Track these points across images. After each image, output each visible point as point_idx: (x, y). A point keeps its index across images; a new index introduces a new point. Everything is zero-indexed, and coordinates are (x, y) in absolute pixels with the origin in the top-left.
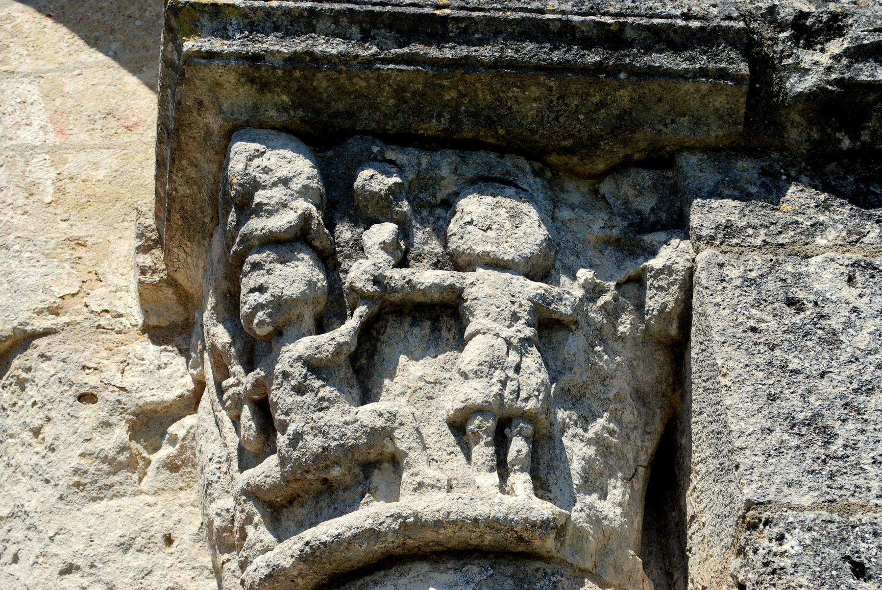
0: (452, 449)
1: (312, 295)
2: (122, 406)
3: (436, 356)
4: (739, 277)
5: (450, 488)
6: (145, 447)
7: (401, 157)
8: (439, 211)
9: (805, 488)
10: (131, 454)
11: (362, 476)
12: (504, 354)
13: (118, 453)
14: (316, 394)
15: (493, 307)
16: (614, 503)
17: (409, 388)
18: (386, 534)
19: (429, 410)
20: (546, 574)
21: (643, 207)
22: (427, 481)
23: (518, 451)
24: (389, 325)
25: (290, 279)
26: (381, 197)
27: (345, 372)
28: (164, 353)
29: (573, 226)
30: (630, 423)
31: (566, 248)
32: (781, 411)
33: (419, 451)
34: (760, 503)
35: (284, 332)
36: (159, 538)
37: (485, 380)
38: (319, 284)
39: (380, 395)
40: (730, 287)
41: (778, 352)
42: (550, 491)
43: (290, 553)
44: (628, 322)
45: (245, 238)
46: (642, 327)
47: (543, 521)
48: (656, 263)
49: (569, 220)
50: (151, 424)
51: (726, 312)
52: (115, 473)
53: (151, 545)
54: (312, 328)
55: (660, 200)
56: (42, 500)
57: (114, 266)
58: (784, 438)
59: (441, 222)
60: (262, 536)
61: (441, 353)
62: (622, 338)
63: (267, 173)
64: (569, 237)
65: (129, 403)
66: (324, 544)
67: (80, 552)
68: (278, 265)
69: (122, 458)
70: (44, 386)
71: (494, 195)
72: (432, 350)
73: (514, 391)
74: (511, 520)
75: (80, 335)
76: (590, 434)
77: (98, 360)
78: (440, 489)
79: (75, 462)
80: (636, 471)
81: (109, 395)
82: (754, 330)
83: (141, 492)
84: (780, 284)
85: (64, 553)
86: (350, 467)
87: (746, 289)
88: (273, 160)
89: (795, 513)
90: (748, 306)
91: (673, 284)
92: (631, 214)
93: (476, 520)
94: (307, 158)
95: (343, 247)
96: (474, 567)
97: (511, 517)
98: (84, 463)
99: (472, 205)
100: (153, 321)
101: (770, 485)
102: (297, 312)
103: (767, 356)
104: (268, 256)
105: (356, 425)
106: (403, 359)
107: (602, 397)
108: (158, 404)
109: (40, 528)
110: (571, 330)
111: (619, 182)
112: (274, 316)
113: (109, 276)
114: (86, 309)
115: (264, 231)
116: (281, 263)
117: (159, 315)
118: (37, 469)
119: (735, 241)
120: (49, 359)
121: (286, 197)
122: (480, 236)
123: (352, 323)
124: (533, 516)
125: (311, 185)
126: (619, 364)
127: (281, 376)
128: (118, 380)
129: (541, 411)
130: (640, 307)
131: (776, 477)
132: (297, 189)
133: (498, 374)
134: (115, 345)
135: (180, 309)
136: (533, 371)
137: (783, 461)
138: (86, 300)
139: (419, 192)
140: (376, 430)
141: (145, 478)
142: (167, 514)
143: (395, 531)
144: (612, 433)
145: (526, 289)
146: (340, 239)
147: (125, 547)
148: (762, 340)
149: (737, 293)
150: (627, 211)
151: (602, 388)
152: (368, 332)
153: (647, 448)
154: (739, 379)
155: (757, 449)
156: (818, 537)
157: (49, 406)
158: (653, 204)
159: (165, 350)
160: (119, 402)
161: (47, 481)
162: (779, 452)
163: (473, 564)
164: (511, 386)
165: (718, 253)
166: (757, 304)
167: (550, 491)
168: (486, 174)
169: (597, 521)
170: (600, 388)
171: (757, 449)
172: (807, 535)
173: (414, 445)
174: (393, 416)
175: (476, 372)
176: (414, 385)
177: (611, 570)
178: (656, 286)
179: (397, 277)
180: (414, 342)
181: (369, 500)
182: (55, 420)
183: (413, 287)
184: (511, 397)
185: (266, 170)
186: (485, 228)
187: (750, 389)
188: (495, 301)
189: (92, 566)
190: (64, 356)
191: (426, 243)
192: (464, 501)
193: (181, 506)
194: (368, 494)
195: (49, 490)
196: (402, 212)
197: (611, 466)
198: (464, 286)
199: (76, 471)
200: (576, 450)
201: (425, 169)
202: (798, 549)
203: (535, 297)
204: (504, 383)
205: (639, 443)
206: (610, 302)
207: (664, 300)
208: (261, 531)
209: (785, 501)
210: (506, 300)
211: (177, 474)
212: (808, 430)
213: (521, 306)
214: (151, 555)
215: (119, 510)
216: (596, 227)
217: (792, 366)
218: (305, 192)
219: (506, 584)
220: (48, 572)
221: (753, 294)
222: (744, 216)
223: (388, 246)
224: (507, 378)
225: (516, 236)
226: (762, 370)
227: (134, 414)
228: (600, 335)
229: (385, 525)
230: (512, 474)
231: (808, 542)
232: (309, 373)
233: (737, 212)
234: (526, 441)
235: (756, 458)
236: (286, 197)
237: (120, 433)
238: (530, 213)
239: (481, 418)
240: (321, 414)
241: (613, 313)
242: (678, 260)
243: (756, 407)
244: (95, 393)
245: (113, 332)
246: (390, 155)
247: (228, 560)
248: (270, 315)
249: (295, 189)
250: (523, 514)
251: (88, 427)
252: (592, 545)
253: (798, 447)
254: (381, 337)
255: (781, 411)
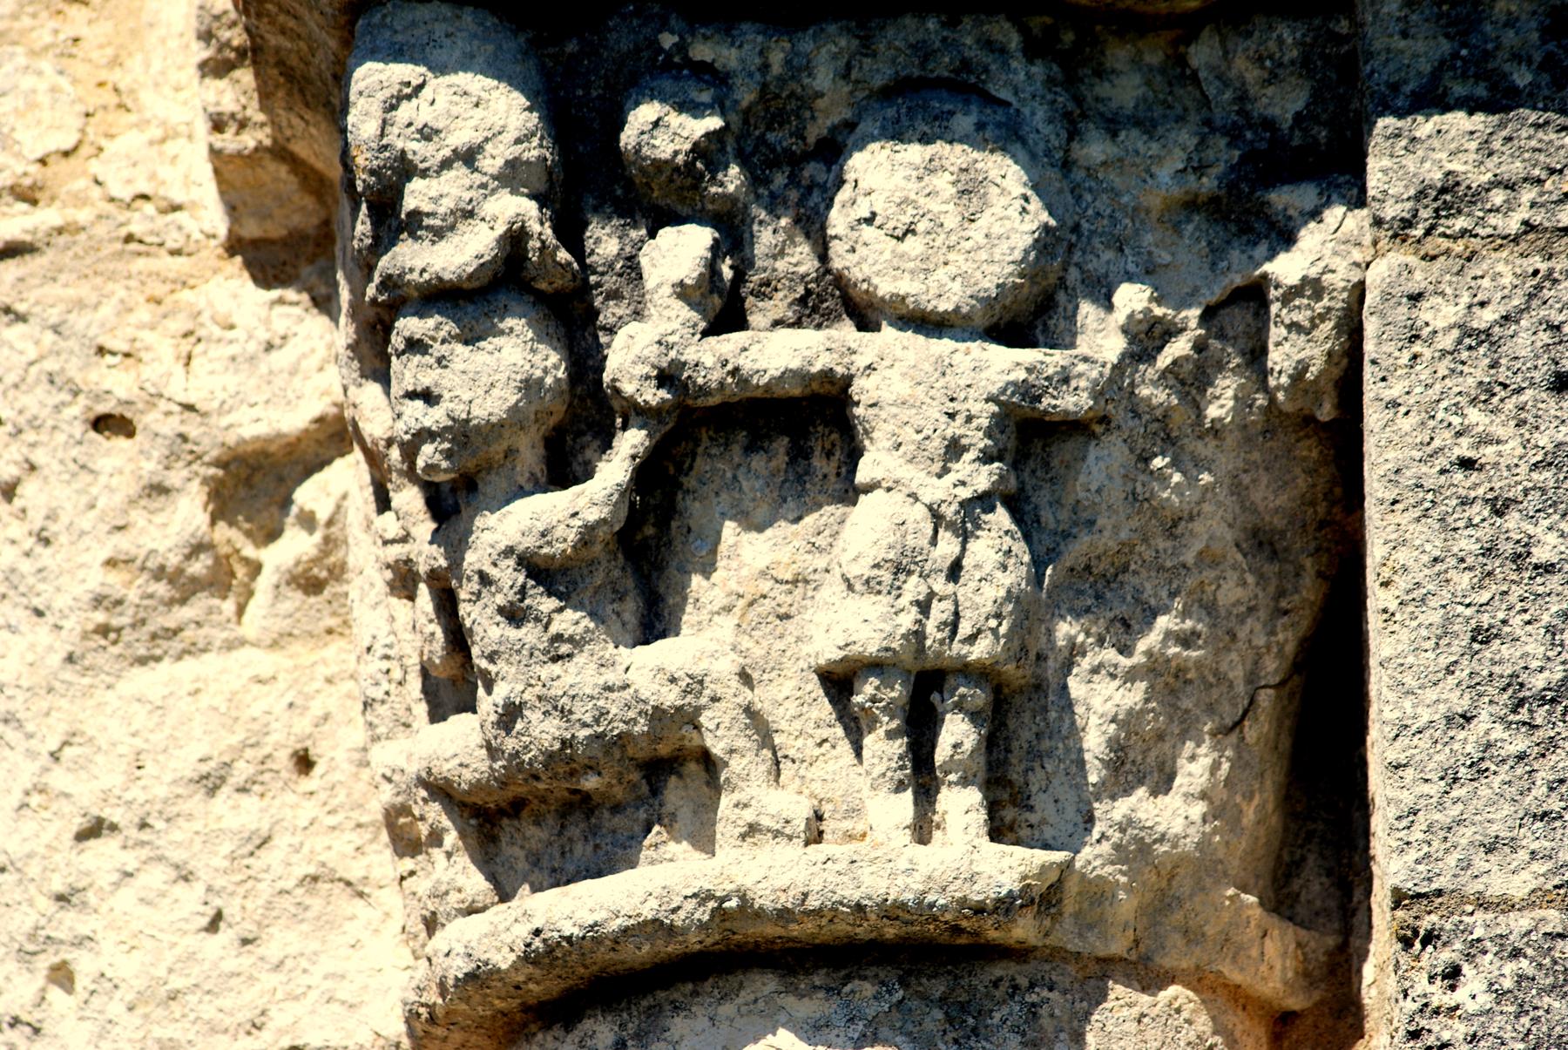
0: (825, 733)
1: (533, 408)
2: (189, 446)
3: (800, 518)
4: (1451, 327)
5: (815, 836)
6: (248, 534)
7: (725, 52)
8: (812, 170)
9: (1523, 855)
10: (217, 559)
11: (645, 789)
12: (924, 542)
13: (188, 557)
14: (546, 628)
15: (909, 430)
16: (1186, 795)
17: (740, 596)
18: (684, 931)
19: (780, 645)
20: (1016, 988)
21: (1277, 111)
22: (766, 822)
23: (956, 746)
24: (700, 450)
25: (485, 380)
26: (677, 169)
27: (610, 570)
28: (279, 309)
29: (1114, 178)
30: (1238, 602)
31: (1092, 232)
32: (1497, 670)
33: (750, 756)
34: (1419, 896)
35: (480, 486)
36: (283, 760)
37: (885, 600)
38: (549, 380)
39: (683, 611)
40: (1427, 353)
41: (1513, 520)
42: (1031, 809)
43: (508, 938)
44: (1230, 393)
45: (388, 283)
46: (1261, 400)
47: (999, 900)
48: (1286, 268)
49: (1104, 163)
50: (256, 483)
51: (1414, 419)
52: (183, 601)
53: (267, 777)
54: (539, 469)
55: (1316, 97)
56: (30, 658)
57: (157, 65)
58: (1493, 736)
59: (816, 197)
60: (461, 881)
61: (810, 511)
62: (1216, 430)
63: (428, 139)
64: (1103, 204)
65: (206, 441)
66: (569, 939)
67: (117, 792)
68: (460, 348)
69: (199, 567)
70: (16, 386)
71: (925, 140)
72: (791, 504)
73: (945, 623)
74: (932, 905)
75: (88, 261)
76: (1138, 658)
77: (130, 332)
78: (790, 838)
79: (97, 579)
80: (1252, 701)
81: (157, 423)
82: (1467, 464)
83: (243, 642)
84: (1545, 337)
85: (85, 791)
86: (620, 773)
87: (1465, 355)
88: (441, 103)
89: (1490, 915)
90: (1463, 400)
91: (1323, 317)
92: (1250, 127)
93: (859, 908)
94: (517, 88)
95: (603, 274)
96: (867, 985)
97: (930, 898)
98: (115, 582)
99: (880, 173)
100: (251, 230)
101: (1447, 851)
102: (505, 445)
103: (1485, 533)
104: (437, 328)
105: (627, 694)
106: (729, 529)
107: (1169, 564)
108: (268, 440)
109: (30, 727)
110: (1093, 435)
111: (1230, 45)
112: (456, 458)
113: (147, 97)
114: (96, 192)
115: (426, 276)
116: (466, 343)
117: (264, 216)
118: (15, 579)
119: (1460, 223)
120: (21, 318)
121: (472, 194)
122: (887, 255)
123: (614, 470)
124: (980, 892)
125: (525, 156)
126: (1207, 489)
127: (476, 578)
128: (179, 389)
129: (1004, 657)
130: (1256, 356)
131: (1462, 830)
132: (494, 171)
133: (913, 587)
134: (168, 287)
135: (309, 202)
136: (995, 559)
137: (1484, 792)
138: (95, 167)
139: (770, 128)
140: (664, 711)
141: (252, 604)
142: (299, 702)
143: (702, 926)
144: (1186, 640)
145: (984, 375)
146: (594, 258)
147: (210, 783)
148: (1480, 491)
149: (1443, 368)
150: (1243, 125)
151: (1169, 544)
152: (655, 484)
153: (1281, 646)
154: (1415, 594)
155: (1432, 765)
156: (1530, 971)
157: (30, 436)
158: (1299, 105)
159: (281, 301)
160: (184, 438)
161: (39, 613)
162: (1479, 770)
163: (865, 978)
164: (940, 612)
165: (1413, 260)
166: (1486, 394)
167: (1031, 809)
168: (916, 72)
169: (1140, 850)
170: (1162, 544)
171: (1432, 765)
172: (1510, 967)
173: (741, 743)
174: (697, 683)
175: (867, 582)
176: (750, 591)
177: (1177, 939)
178: (1287, 321)
179: (709, 364)
180: (752, 489)
181: (659, 839)
182: (46, 472)
183: (744, 382)
184: (939, 636)
185: (427, 134)
186: (899, 233)
187: (1436, 617)
188: (920, 396)
189: (143, 825)
190: (54, 316)
191: (782, 253)
192: (837, 867)
193: (329, 681)
194: (656, 828)
195: (41, 633)
196: (724, 196)
197: (1187, 711)
198: (853, 371)
199: (98, 601)
200: (1096, 702)
201: (780, 78)
202: (1486, 1000)
203: (1003, 391)
204: (924, 607)
205: (1260, 641)
206: (1187, 358)
207: (1302, 355)
208: (459, 867)
209: (1473, 887)
210: (935, 413)
211: (320, 599)
212: (1550, 713)
213: (969, 419)
214: (267, 799)
215: (197, 691)
216: (1164, 173)
217: (1540, 555)
218: (512, 176)
219: (928, 1019)
220: (53, 829)
221: (1478, 372)
222: (1490, 155)
223: (689, 291)
224: (931, 595)
225: (968, 245)
226: (1470, 569)
227: (217, 463)
228: (1163, 432)
229: (682, 914)
230: (944, 790)
231: (1508, 984)
232: (531, 582)
233: (1473, 145)
234: (972, 721)
235: (1426, 789)
236: (472, 194)
237: (189, 513)
238: (1006, 175)
239: (877, 682)
240: (556, 668)
241: (1192, 380)
242: (1336, 262)
243: (1444, 661)
244: (128, 415)
245: (163, 252)
246: (702, 51)
247: (412, 873)
248: (448, 454)
249: (491, 171)
250: (957, 890)
251: (118, 499)
252: (1126, 903)
253: (1521, 757)
254: (684, 480)
255: (1497, 670)
